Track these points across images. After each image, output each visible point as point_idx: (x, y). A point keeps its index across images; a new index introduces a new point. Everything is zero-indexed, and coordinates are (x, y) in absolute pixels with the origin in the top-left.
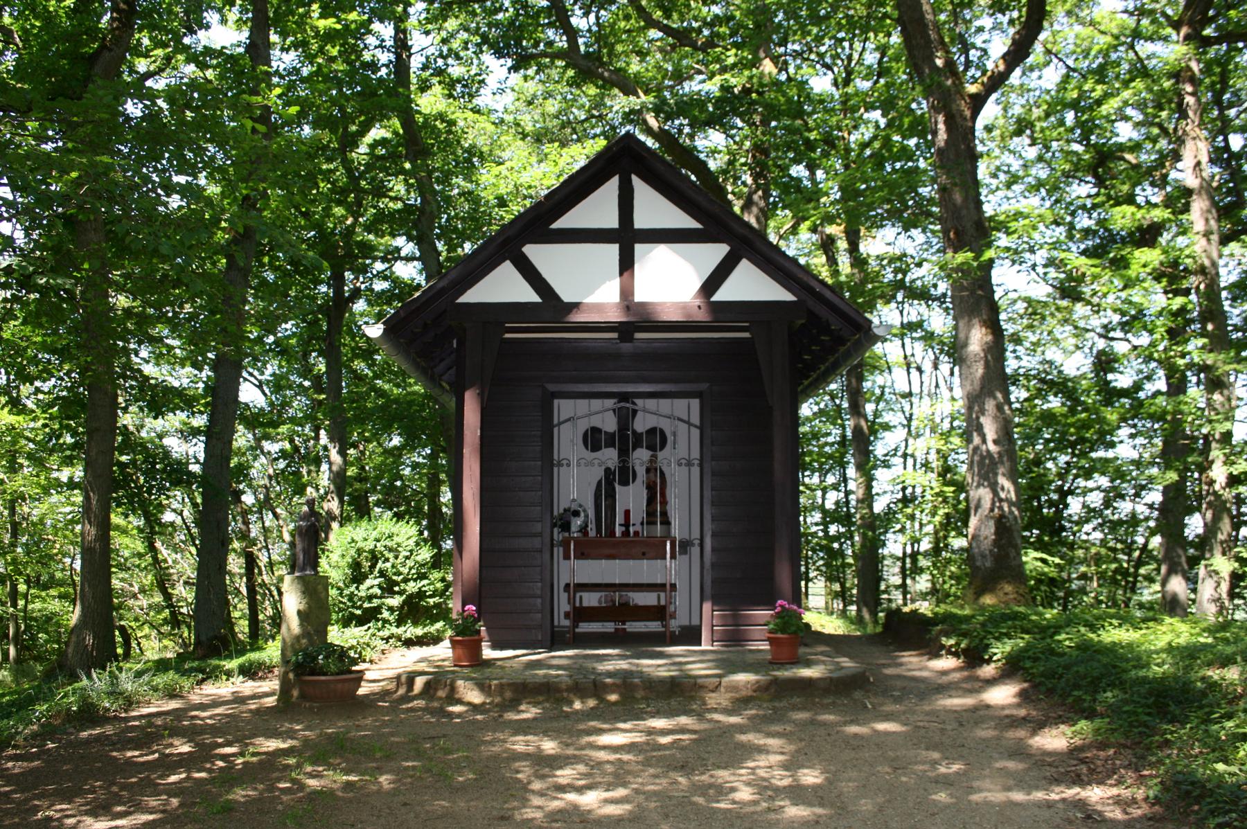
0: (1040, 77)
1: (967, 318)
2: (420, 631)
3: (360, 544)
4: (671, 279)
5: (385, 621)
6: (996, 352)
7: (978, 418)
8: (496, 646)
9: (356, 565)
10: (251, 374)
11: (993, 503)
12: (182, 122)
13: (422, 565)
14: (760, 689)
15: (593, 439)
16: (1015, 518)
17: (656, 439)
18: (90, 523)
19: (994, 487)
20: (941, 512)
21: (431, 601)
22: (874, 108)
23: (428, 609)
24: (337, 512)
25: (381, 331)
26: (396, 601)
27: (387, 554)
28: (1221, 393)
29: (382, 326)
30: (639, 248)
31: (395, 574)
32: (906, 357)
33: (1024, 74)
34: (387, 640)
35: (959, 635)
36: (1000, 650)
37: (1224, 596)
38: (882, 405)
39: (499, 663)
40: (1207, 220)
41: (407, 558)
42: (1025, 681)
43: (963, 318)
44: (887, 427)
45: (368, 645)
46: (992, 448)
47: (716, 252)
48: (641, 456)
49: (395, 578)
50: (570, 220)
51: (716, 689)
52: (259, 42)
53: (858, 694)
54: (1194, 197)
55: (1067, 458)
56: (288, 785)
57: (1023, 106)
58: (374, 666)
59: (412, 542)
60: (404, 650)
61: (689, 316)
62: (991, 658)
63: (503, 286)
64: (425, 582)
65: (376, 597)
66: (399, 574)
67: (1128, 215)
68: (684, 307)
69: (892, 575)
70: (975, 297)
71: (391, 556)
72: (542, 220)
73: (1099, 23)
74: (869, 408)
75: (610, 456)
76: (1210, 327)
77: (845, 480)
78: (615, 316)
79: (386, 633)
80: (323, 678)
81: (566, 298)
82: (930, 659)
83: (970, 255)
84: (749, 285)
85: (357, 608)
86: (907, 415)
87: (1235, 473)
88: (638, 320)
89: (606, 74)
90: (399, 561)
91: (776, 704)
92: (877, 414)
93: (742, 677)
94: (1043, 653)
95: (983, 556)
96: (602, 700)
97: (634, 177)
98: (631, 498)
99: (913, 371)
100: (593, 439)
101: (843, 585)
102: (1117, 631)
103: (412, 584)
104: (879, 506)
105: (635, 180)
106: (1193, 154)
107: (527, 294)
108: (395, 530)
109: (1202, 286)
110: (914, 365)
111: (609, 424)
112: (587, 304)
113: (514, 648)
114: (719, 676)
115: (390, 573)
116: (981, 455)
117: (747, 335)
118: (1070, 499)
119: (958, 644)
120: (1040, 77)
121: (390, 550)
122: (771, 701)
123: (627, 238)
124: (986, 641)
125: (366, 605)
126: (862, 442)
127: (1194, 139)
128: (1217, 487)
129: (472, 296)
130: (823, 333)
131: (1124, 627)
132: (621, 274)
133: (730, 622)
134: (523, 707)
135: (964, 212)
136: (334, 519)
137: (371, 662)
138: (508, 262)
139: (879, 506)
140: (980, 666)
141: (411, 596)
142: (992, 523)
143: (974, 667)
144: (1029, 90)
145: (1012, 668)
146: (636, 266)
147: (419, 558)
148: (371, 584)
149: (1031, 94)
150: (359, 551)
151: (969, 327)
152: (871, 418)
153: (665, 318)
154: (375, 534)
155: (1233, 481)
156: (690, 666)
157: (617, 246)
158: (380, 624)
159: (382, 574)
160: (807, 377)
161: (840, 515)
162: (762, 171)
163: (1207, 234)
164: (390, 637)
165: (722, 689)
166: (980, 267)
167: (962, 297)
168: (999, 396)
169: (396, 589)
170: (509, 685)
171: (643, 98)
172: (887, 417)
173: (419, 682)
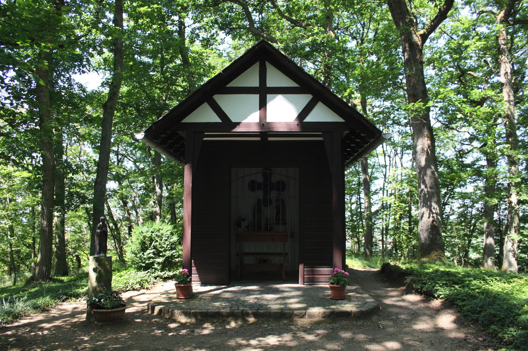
0: (437, 43)
3: (145, 234)
4: (283, 112)
5: (156, 269)
7: (423, 177)
9: (143, 243)
10: (132, 158)
15: (253, 186)
16: (440, 221)
17: (281, 186)
18: (44, 220)
21: (177, 260)
22: (372, 54)
23: (176, 263)
25: (143, 136)
26: (161, 260)
28: (515, 167)
30: (268, 96)
31: (160, 248)
32: (384, 152)
33: (431, 41)
34: (156, 278)
37: (515, 249)
38: (374, 170)
40: (509, 96)
41: (166, 240)
44: (376, 178)
47: (305, 99)
48: (273, 194)
49: (160, 249)
50: (235, 83)
51: (303, 316)
52: (118, 19)
54: (505, 86)
55: (446, 191)
56: (140, 320)
57: (430, 54)
58: (148, 292)
62: (438, 296)
63: (205, 115)
64: (174, 251)
66: (162, 247)
67: (478, 94)
68: (288, 124)
69: (377, 235)
70: (421, 124)
72: (224, 83)
73: (461, 20)
74: (370, 170)
75: (260, 194)
76: (510, 140)
79: (156, 274)
81: (234, 120)
84: (321, 114)
85: (143, 263)
87: (522, 200)
88: (266, 131)
89: (265, 35)
90: (162, 242)
91: (334, 325)
92: (372, 173)
94: (466, 296)
96: (245, 321)
97: (267, 62)
98: (269, 212)
99: (386, 157)
100: (253, 186)
101: (358, 239)
103: (168, 252)
104: (374, 209)
106: (504, 69)
107: (215, 119)
110: (387, 154)
111: (260, 179)
115: (159, 246)
116: (424, 194)
117: (321, 139)
120: (437, 43)
122: (331, 323)
123: (264, 93)
125: (147, 262)
126: (367, 184)
127: (505, 63)
128: (513, 205)
129: (189, 119)
130: (359, 136)
132: (260, 109)
134: (205, 325)
135: (417, 86)
136: (157, 215)
137: (147, 289)
141: (168, 257)
145: (450, 304)
147: (171, 240)
148: (150, 252)
150: (145, 237)
154: (151, 230)
155: (520, 202)
157: (258, 96)
158: (153, 270)
159: (155, 247)
160: (348, 159)
162: (328, 75)
163: (509, 102)
164: (158, 277)
165: (307, 317)
168: (433, 167)
169: (161, 254)
171: (280, 45)
172: (376, 175)
173: (157, 309)
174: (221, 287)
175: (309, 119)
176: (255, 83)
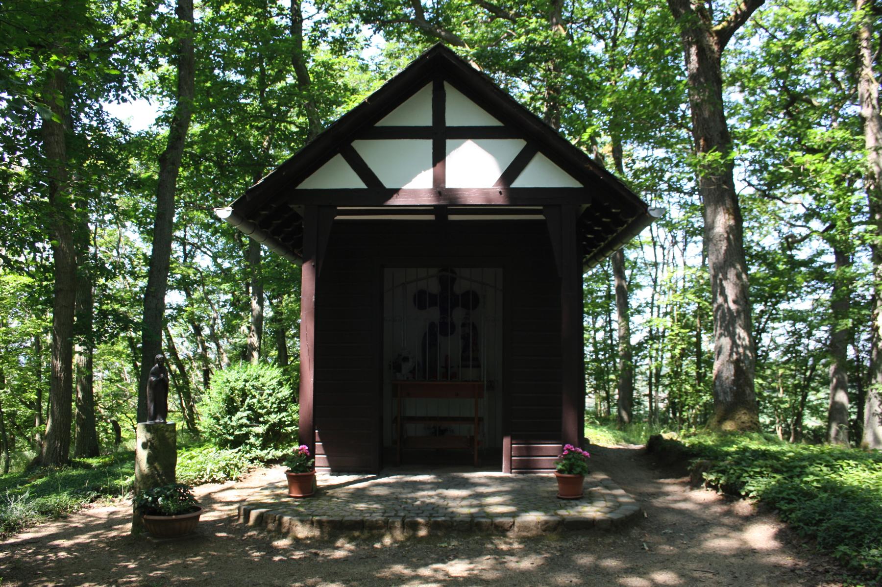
0: (748, 44)
1: (713, 207)
2: (279, 453)
3: (232, 384)
4: (475, 170)
5: (252, 445)
6: (736, 232)
8: (336, 470)
9: (229, 400)
11: (732, 349)
12: (305, 140)
13: (281, 402)
14: (547, 527)
15: (422, 300)
17: (471, 300)
19: (732, 335)
20: (679, 347)
21: (289, 429)
23: (288, 435)
24: (257, 345)
25: (230, 213)
26: (261, 429)
27: (254, 392)
29: (230, 209)
30: (449, 143)
31: (260, 408)
34: (252, 461)
35: (718, 472)
36: (756, 486)
39: (330, 492)
41: (270, 395)
42: (782, 521)
43: (709, 205)
44: (639, 286)
45: (236, 465)
46: (733, 307)
47: (513, 147)
48: (458, 315)
49: (260, 411)
53: (635, 532)
54: (867, 123)
57: (736, 64)
59: (274, 382)
60: (264, 470)
61: (489, 200)
62: (747, 494)
63: (338, 176)
64: (284, 414)
65: (246, 426)
66: (263, 407)
68: (485, 192)
69: (641, 386)
70: (718, 189)
71: (256, 394)
74: (627, 273)
77: (610, 322)
78: (427, 200)
80: (162, 518)
81: (388, 184)
82: (692, 489)
83: (718, 154)
86: (654, 277)
88: (447, 201)
89: (443, 33)
90: (263, 397)
93: (534, 517)
95: (725, 393)
97: (446, 84)
99: (658, 247)
101: (607, 393)
102: (854, 471)
103: (273, 416)
104: (634, 340)
105: (447, 85)
107: (356, 182)
108: (261, 372)
109: (872, 188)
110: (658, 243)
111: (434, 287)
112: (406, 191)
113: (349, 473)
114: (513, 515)
118: (764, 335)
119: (718, 480)
120: (748, 44)
121: (257, 389)
123: (440, 137)
124: (743, 479)
125: (237, 433)
130: (609, 212)
131: (860, 468)
132: (434, 165)
133: (525, 453)
134: (339, 543)
136: (254, 349)
137: (237, 479)
138: (339, 155)
139: (634, 340)
140: (737, 500)
142: (732, 367)
143: (732, 501)
144: (740, 53)
146: (447, 158)
147: (280, 395)
148: (242, 415)
149: (742, 55)
150: (232, 389)
151: (715, 213)
152: (628, 279)
153: (471, 202)
154: (244, 376)
156: (490, 500)
159: (250, 407)
161: (608, 348)
164: (255, 459)
165: (516, 529)
166: (725, 165)
167: (710, 190)
168: (738, 267)
169: (261, 419)
170: (330, 522)
172: (639, 279)
173: (254, 514)
174: (366, 477)
175: (520, 182)
176: (425, 119)
